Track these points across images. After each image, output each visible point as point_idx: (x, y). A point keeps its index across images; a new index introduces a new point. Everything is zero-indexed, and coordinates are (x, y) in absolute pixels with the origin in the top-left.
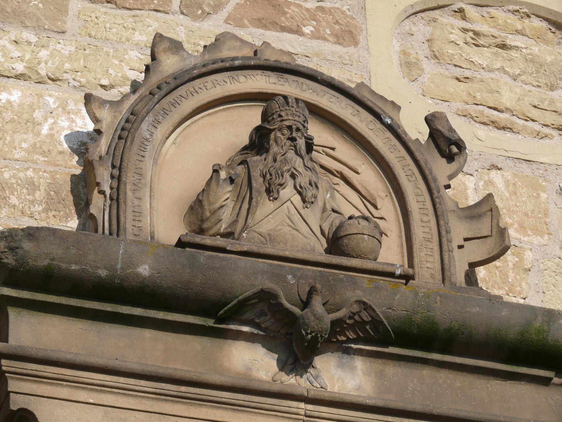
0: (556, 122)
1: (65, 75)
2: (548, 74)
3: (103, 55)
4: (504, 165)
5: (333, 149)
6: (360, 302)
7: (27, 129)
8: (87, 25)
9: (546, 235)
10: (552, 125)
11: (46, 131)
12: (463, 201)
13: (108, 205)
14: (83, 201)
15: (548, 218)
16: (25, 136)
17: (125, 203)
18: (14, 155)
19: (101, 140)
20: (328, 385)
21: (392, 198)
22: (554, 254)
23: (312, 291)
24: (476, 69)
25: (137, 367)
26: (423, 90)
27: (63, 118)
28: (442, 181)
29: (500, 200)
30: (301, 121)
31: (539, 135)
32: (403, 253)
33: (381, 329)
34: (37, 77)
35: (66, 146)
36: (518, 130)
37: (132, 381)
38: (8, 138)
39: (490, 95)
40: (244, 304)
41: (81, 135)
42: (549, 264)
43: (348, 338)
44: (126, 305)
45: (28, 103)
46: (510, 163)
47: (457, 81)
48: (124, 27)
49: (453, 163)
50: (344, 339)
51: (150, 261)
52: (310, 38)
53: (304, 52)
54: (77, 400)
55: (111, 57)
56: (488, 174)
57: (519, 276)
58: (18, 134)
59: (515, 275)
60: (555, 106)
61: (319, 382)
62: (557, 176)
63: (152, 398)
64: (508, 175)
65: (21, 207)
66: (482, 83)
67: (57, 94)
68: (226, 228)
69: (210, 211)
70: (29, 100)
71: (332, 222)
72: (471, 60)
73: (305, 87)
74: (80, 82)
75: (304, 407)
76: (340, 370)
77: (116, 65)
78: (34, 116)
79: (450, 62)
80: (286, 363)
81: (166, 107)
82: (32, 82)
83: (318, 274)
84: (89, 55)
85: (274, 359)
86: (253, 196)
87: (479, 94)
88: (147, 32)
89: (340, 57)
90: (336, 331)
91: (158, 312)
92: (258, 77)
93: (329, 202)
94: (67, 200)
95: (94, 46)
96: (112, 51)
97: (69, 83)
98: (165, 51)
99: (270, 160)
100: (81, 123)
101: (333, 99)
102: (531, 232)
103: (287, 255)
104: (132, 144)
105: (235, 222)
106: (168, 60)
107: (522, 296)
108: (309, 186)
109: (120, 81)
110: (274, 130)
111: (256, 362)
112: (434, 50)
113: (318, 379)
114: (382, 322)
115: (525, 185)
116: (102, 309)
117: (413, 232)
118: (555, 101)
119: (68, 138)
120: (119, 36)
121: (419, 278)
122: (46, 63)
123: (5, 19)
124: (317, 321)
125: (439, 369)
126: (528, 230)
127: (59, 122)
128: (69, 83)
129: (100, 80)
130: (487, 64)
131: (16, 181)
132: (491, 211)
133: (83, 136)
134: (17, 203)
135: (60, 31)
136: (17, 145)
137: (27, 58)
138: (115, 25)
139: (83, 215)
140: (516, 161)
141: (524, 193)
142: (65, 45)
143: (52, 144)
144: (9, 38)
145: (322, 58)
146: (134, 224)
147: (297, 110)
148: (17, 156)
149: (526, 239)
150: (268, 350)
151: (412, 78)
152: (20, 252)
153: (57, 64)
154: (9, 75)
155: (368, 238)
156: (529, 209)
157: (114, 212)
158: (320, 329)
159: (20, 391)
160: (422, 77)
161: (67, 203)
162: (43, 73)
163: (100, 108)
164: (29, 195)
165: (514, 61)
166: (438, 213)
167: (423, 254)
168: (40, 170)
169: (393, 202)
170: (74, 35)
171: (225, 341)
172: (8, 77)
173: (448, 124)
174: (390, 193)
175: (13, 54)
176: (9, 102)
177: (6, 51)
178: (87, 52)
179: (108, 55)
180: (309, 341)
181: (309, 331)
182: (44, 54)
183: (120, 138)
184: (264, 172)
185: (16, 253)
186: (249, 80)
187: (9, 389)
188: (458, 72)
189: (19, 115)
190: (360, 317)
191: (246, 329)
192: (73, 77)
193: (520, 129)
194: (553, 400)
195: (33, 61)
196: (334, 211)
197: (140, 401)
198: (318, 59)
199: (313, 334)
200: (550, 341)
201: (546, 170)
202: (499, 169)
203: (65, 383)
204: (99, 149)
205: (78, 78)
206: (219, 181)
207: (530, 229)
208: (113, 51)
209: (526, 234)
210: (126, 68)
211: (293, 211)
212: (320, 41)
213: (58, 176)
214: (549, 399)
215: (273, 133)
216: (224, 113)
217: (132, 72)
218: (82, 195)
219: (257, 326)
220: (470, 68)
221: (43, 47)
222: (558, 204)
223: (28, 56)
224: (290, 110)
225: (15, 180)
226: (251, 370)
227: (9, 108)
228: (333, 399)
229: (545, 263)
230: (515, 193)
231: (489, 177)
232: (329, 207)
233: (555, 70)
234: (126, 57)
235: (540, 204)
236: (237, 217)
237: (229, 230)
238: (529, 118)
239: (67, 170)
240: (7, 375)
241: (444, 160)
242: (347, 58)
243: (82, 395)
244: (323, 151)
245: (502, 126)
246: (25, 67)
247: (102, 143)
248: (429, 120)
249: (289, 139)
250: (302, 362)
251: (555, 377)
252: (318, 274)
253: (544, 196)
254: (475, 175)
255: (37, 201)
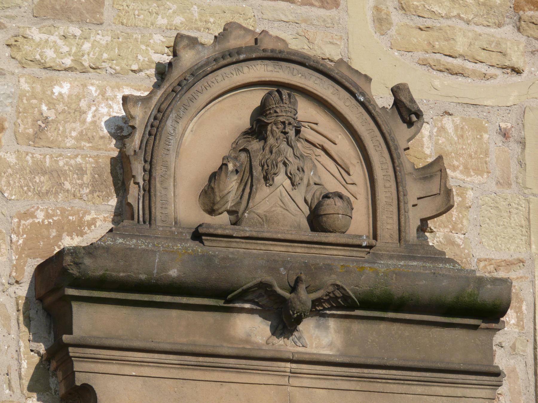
0: (501, 62)
1: (103, 64)
2: (497, 14)
3: (133, 41)
4: (454, 110)
5: (317, 124)
6: (334, 285)
7: (75, 118)
8: (120, 14)
9: (485, 174)
10: (497, 65)
11: (90, 118)
12: (419, 148)
13: (141, 195)
14: (120, 180)
15: (488, 157)
16: (74, 125)
17: (155, 195)
18: (66, 143)
19: (135, 135)
20: (308, 343)
21: (362, 165)
22: (491, 190)
23: (298, 280)
24: (436, 17)
25: (167, 347)
26: (391, 44)
27: (103, 105)
28: (402, 145)
29: (449, 145)
30: (292, 115)
31: (485, 77)
32: (369, 214)
33: (350, 301)
34: (81, 68)
35: (105, 131)
36: (469, 74)
37: (163, 356)
38: (61, 128)
39: (446, 42)
40: (246, 292)
41: (117, 119)
42: (487, 199)
43: (324, 307)
44: (158, 295)
45: (75, 94)
46: (460, 108)
47: (419, 31)
48: (149, 12)
49: (413, 127)
50: (321, 308)
51: (178, 266)
52: (299, 5)
53: (295, 19)
54: (124, 374)
55: (139, 43)
56: (441, 121)
57: (461, 214)
58: (69, 123)
59: (458, 214)
60: (501, 48)
61: (301, 341)
62: (498, 117)
63: (178, 368)
64: (457, 120)
65: (73, 191)
66: (440, 31)
67: (97, 82)
68: (231, 207)
69: (220, 197)
70: (76, 91)
71: (314, 193)
72: (432, 10)
73: (295, 72)
74: (115, 70)
75: (289, 367)
76: (317, 330)
77: (143, 50)
78: (80, 106)
79: (414, 13)
80: (276, 329)
81: (186, 102)
82: (78, 73)
83: (303, 265)
84: (122, 43)
85: (268, 325)
86: (254, 184)
87: (437, 43)
88: (168, 15)
89: (324, 21)
90: (316, 305)
91: (182, 298)
92: (258, 67)
93: (312, 178)
94: (108, 181)
95: (126, 33)
96: (140, 36)
97: (106, 71)
98: (184, 48)
99: (267, 151)
100: (117, 108)
101: (318, 81)
102: (473, 173)
103: (279, 238)
104: (159, 141)
105: (239, 203)
106: (186, 55)
107: (462, 232)
108: (297, 171)
109: (147, 65)
110: (270, 123)
111: (254, 329)
112: (402, 2)
113: (301, 340)
114: (350, 297)
115: (471, 128)
116: (142, 299)
117: (377, 198)
118: (501, 43)
119: (108, 123)
120: (145, 22)
121: (380, 240)
122: (88, 55)
123: (55, 16)
124: (302, 305)
125: (393, 323)
126: (471, 170)
127: (100, 109)
128: (106, 71)
129: (131, 66)
130: (445, 13)
131: (69, 168)
132: (441, 171)
133: (118, 120)
134: (70, 188)
135: (99, 23)
136: (68, 134)
137: (73, 51)
138: (142, 12)
139: (120, 194)
140: (465, 106)
141: (470, 135)
142: (103, 36)
143: (95, 130)
144: (59, 33)
145: (309, 23)
146: (162, 212)
147: (289, 106)
148: (68, 145)
149: (469, 179)
150: (263, 318)
151: (382, 32)
152: (82, 266)
153: (97, 54)
154: (60, 69)
155: (342, 217)
156: (472, 151)
157: (147, 202)
158: (304, 310)
159: (82, 371)
160: (391, 30)
161: (108, 183)
162: (86, 64)
163: (134, 106)
164: (79, 179)
165: (468, 7)
166: (398, 180)
167: (384, 217)
168: (86, 156)
169: (363, 168)
170: (109, 25)
171: (232, 314)
172: (59, 71)
173: (409, 96)
174: (360, 160)
175: (63, 50)
176: (60, 94)
177: (57, 47)
178: (120, 40)
179: (137, 41)
180: (295, 319)
181: (295, 312)
182: (87, 46)
183: (150, 134)
184: (263, 162)
185: (80, 267)
186: (251, 70)
187: (75, 370)
188: (421, 22)
189: (69, 105)
190: (334, 294)
191: (247, 306)
192: (110, 65)
193: (470, 73)
194: (480, 340)
195: (78, 54)
196: (315, 184)
197: (169, 371)
198: (306, 25)
199: (298, 314)
200: (479, 301)
201: (489, 112)
202: (450, 115)
203: (114, 362)
204: (133, 144)
205: (114, 66)
206: (227, 173)
207: (473, 170)
208: (141, 36)
209: (469, 175)
210: (151, 52)
211: (285, 193)
212: (307, 7)
213: (100, 160)
214: (477, 339)
215: (270, 125)
216: (231, 99)
217: (157, 55)
218: (119, 176)
219: (257, 304)
220: (431, 17)
221: (85, 39)
222: (497, 143)
223: (74, 50)
224: (284, 106)
225: (68, 167)
226: (250, 336)
227: (61, 100)
228: (311, 360)
229: (483, 199)
230: (462, 136)
231: (442, 124)
232: (312, 182)
233: (503, 10)
234: (152, 41)
235: (482, 144)
236: (241, 198)
237: (234, 209)
238: (478, 61)
239: (107, 153)
240: (73, 359)
241: (405, 125)
242: (329, 21)
243: (127, 370)
244: (309, 126)
245: (455, 72)
246: (72, 60)
247: (136, 138)
248: (395, 91)
249: (282, 132)
250: (289, 328)
251: (483, 322)
252: (303, 265)
253: (486, 136)
254: (430, 123)
255: (85, 184)
